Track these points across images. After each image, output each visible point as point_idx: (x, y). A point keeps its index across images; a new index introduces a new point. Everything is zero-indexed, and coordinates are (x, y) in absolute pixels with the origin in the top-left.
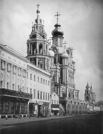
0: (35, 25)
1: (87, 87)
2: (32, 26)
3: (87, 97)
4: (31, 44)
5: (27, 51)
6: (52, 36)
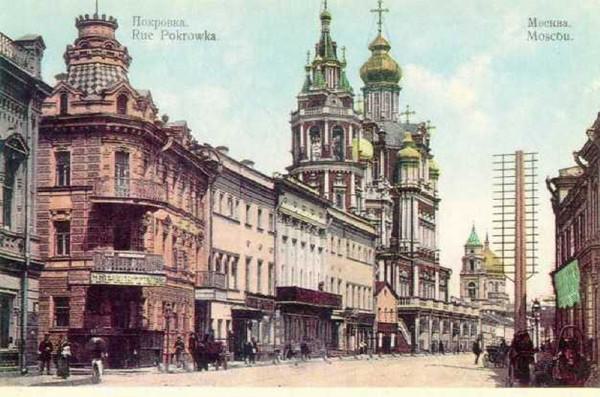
0: (315, 63)
1: (470, 247)
2: (305, 64)
3: (472, 284)
4: (307, 125)
5: (290, 148)
6: (363, 85)
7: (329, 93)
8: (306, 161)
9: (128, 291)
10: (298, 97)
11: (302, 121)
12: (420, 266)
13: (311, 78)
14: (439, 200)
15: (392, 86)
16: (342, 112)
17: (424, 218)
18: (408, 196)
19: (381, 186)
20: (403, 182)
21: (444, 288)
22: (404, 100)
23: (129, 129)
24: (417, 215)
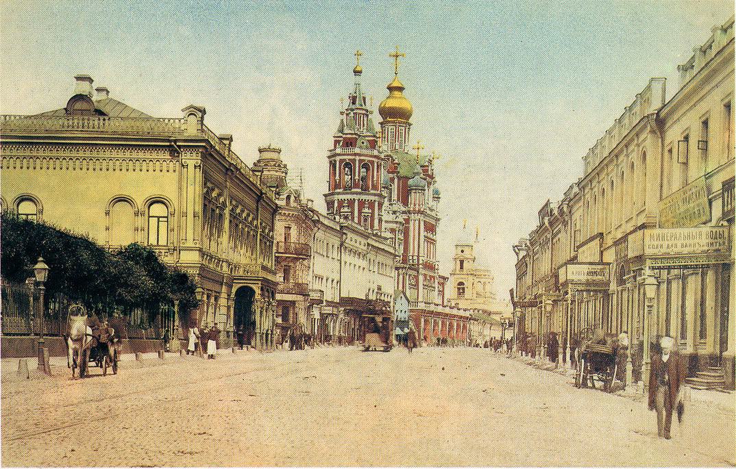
9: (85, 255)
12: (425, 275)
19: (395, 208)
21: (442, 293)
24: (423, 233)
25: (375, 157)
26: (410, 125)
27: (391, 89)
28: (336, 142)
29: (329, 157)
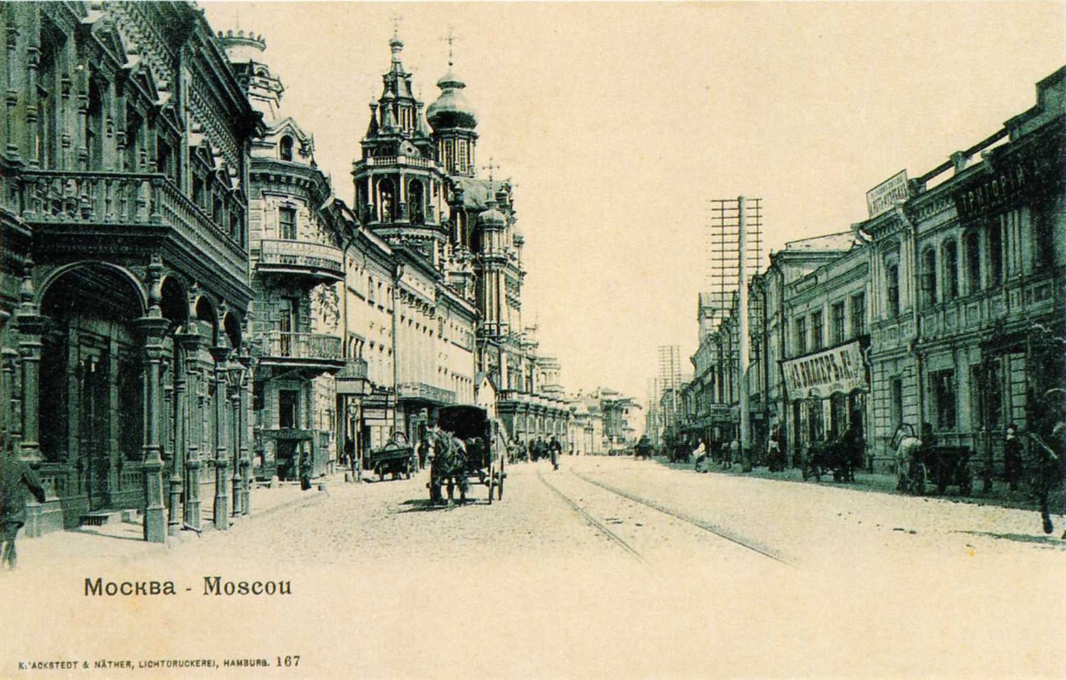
7: (403, 139)
8: (375, 223)
10: (363, 143)
11: (370, 173)
13: (378, 118)
14: (523, 274)
15: (469, 134)
16: (420, 163)
17: (511, 294)
18: (494, 268)
20: (486, 251)
22: (481, 154)
23: (276, 176)
25: (431, 170)
26: (475, 137)
27: (442, 85)
28: (365, 151)
29: (353, 173)
